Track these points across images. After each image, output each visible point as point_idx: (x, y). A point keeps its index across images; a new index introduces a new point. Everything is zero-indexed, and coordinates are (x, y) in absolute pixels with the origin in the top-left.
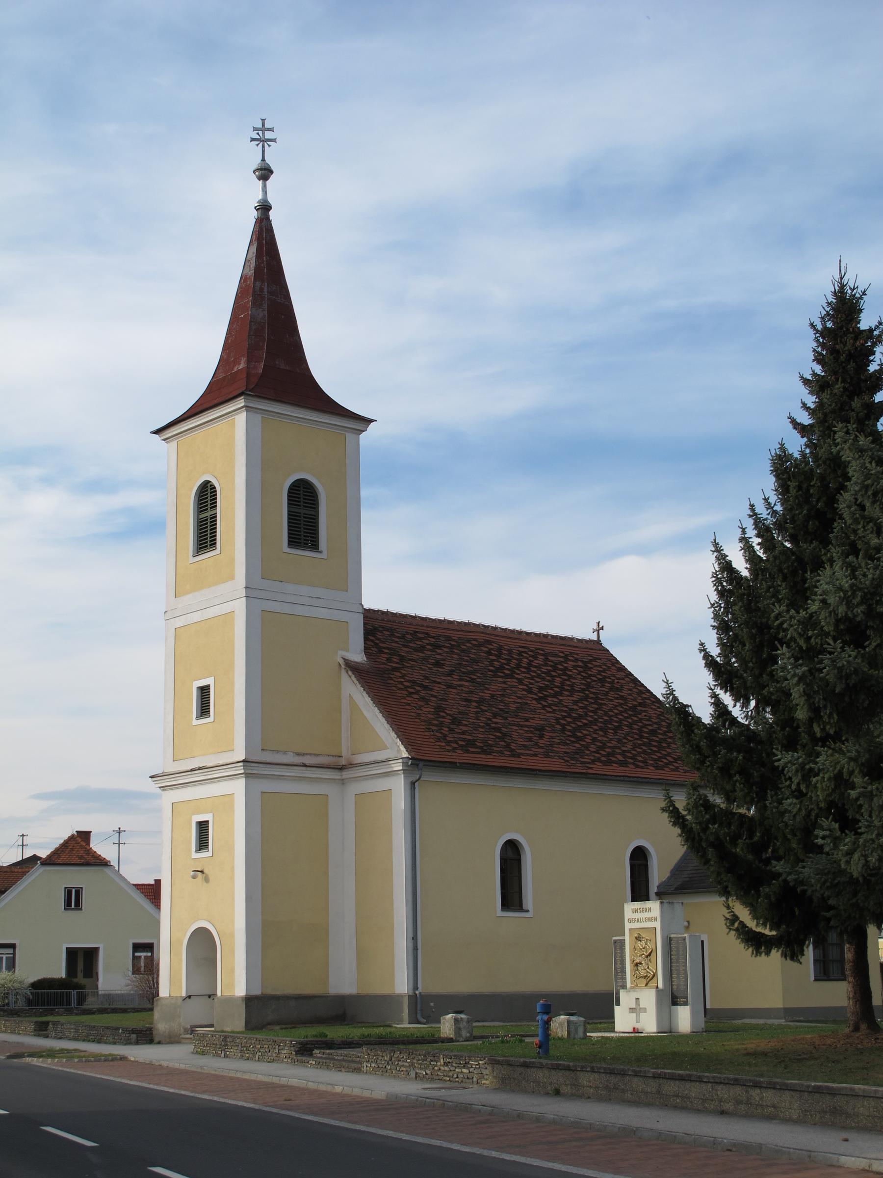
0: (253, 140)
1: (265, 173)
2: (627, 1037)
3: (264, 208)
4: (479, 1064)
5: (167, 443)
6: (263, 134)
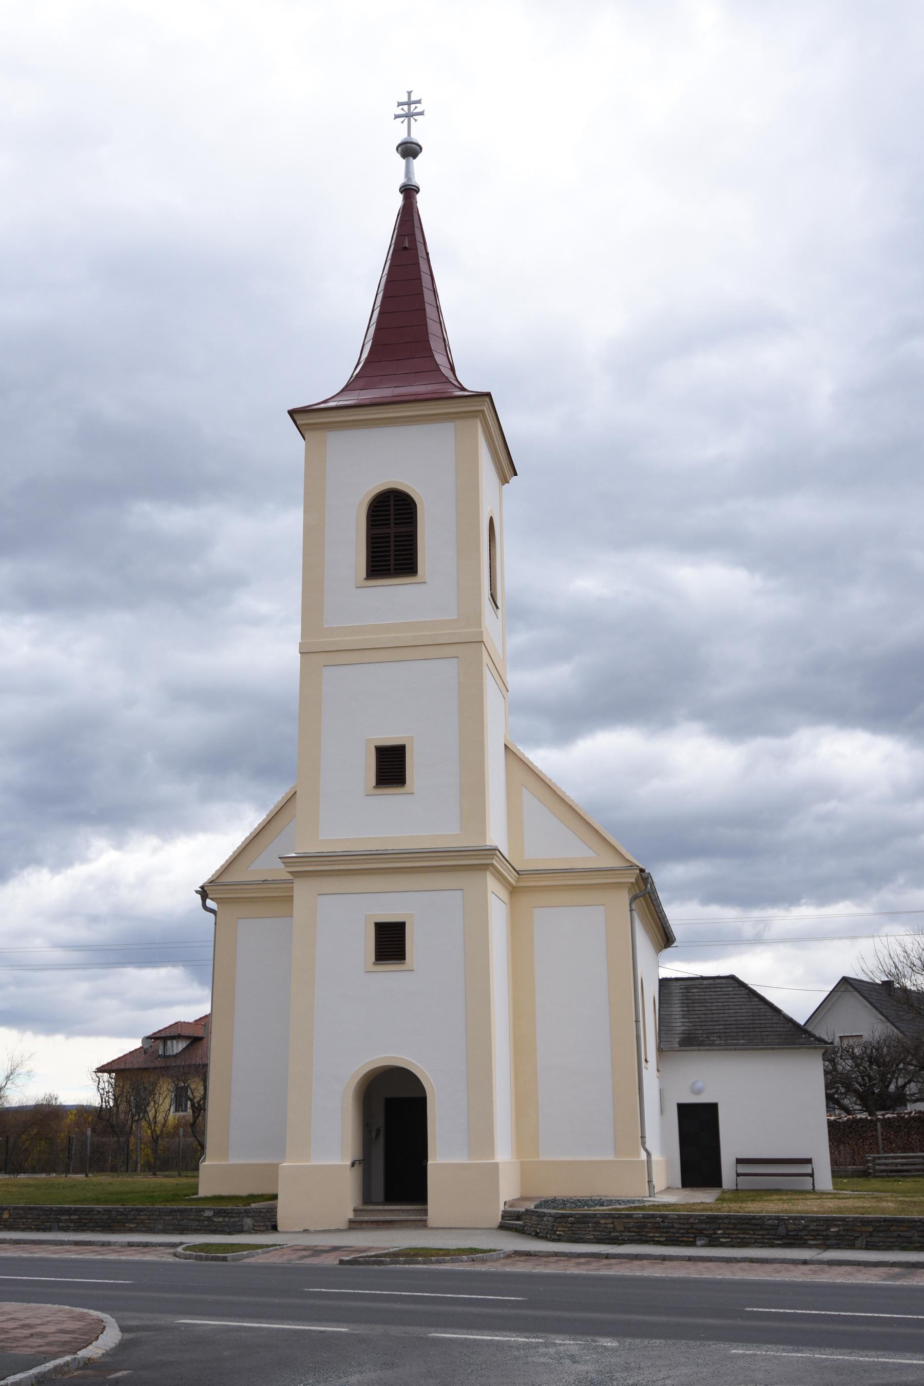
0: (397, 117)
1: (409, 150)
2: (400, 221)
3: (409, 192)
4: (874, 1164)
5: (286, 867)
6: (409, 109)
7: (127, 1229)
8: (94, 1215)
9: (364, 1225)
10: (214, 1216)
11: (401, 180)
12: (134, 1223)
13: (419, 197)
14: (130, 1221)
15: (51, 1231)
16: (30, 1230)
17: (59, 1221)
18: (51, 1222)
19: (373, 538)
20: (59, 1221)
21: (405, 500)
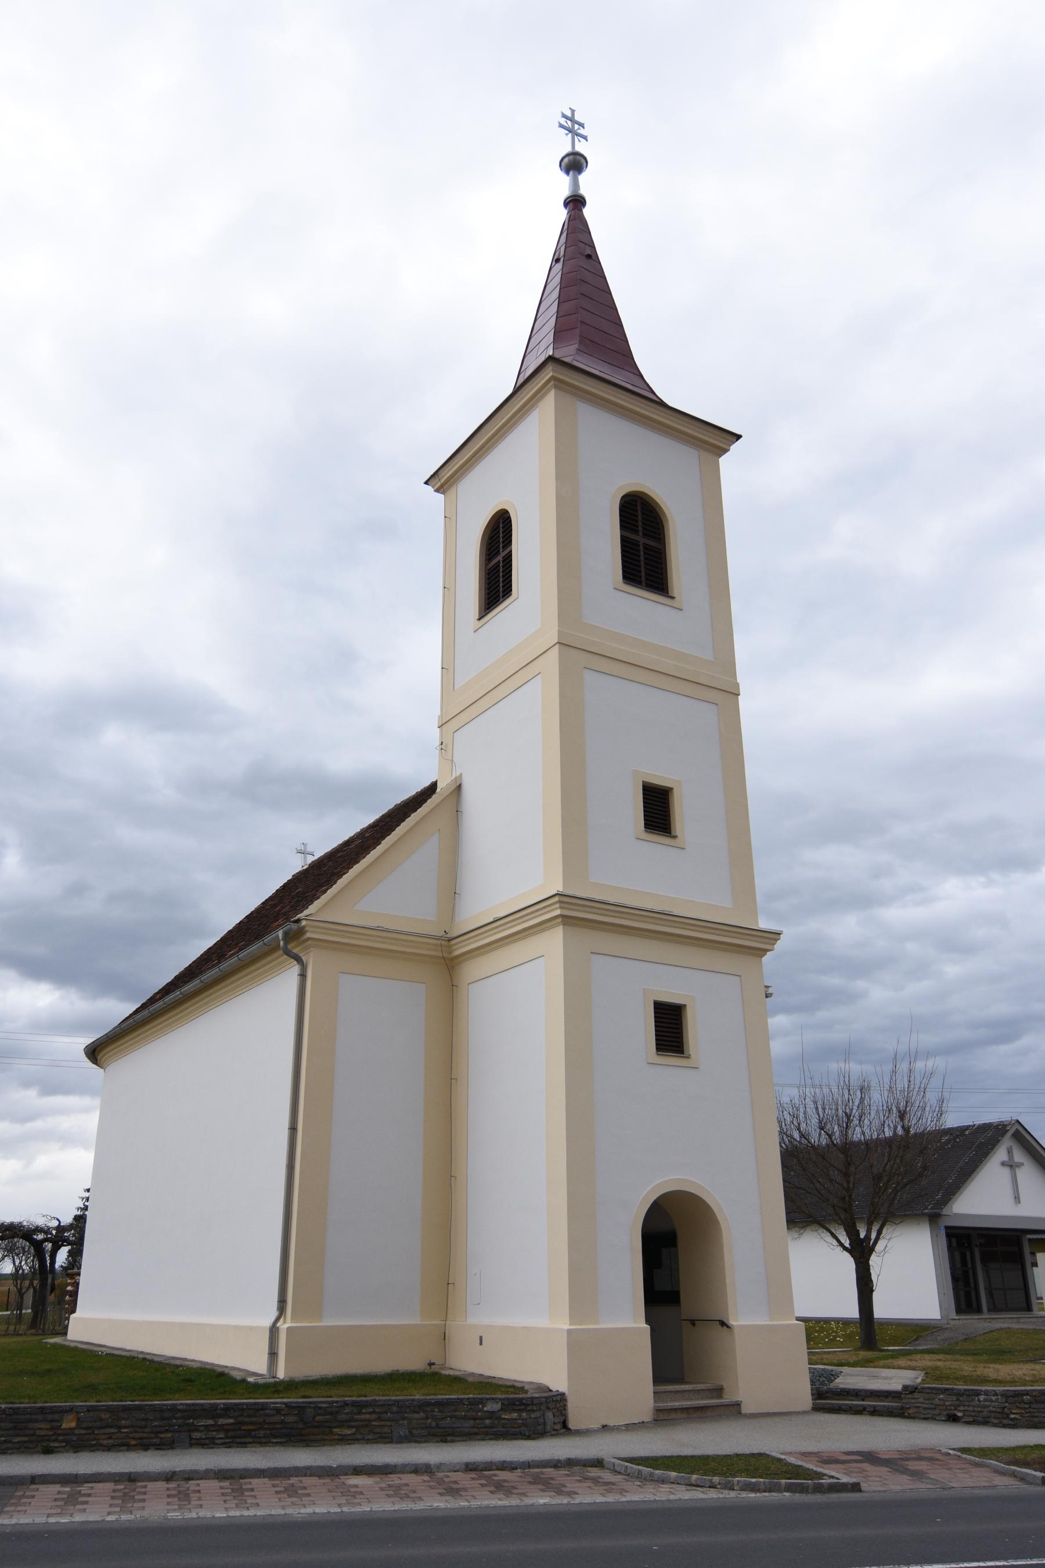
3: (575, 203)
11: (565, 192)
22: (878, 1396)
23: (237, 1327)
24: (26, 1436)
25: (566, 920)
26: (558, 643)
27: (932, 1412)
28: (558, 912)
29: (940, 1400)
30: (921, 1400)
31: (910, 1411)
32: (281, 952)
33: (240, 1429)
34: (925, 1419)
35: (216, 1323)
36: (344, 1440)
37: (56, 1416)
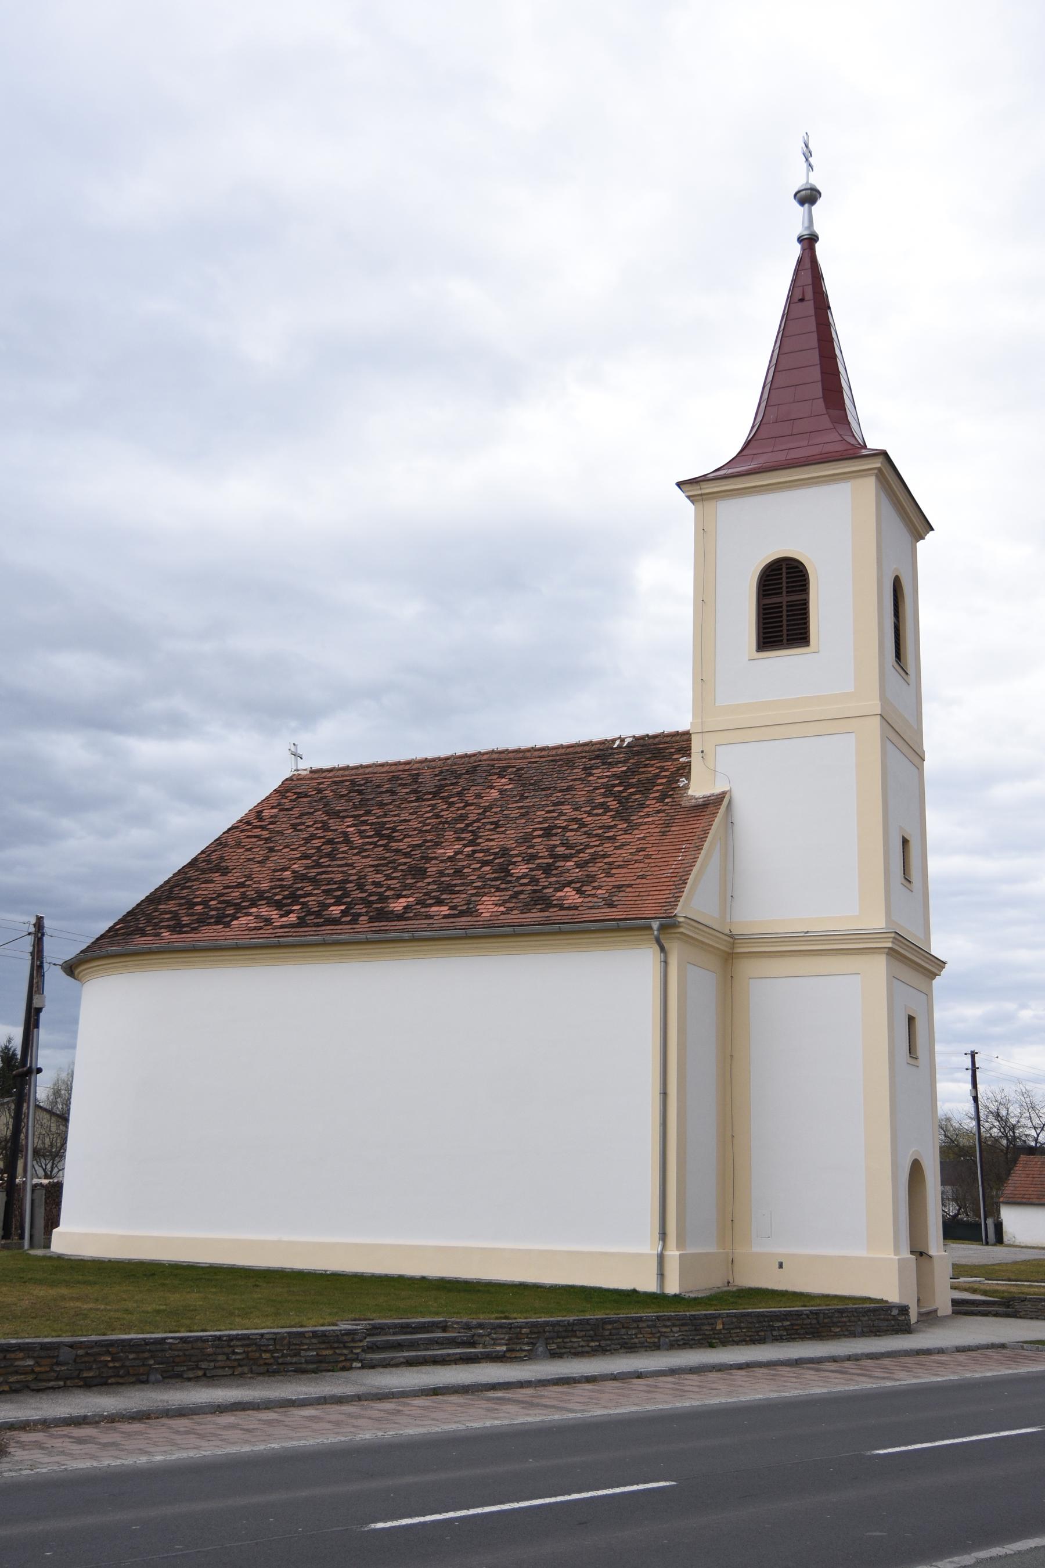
1: (808, 197)
3: (809, 241)
7: (833, 1334)
8: (804, 1319)
9: (585, 1354)
10: (898, 1314)
11: (799, 230)
12: (838, 1327)
13: (818, 246)
14: (835, 1324)
15: (764, 1343)
16: (744, 1343)
17: (773, 1328)
18: (765, 1331)
19: (764, 609)
20: (773, 1328)
21: (797, 567)
22: (988, 1304)
23: (560, 1251)
24: (700, 1335)
25: (891, 952)
26: (880, 715)
27: (1036, 1314)
28: (890, 945)
29: (1042, 1306)
30: (1029, 1306)
31: (1021, 1314)
32: (653, 937)
33: (793, 1329)
34: (1032, 1318)
35: (485, 1246)
36: (836, 1336)
37: (713, 1321)
